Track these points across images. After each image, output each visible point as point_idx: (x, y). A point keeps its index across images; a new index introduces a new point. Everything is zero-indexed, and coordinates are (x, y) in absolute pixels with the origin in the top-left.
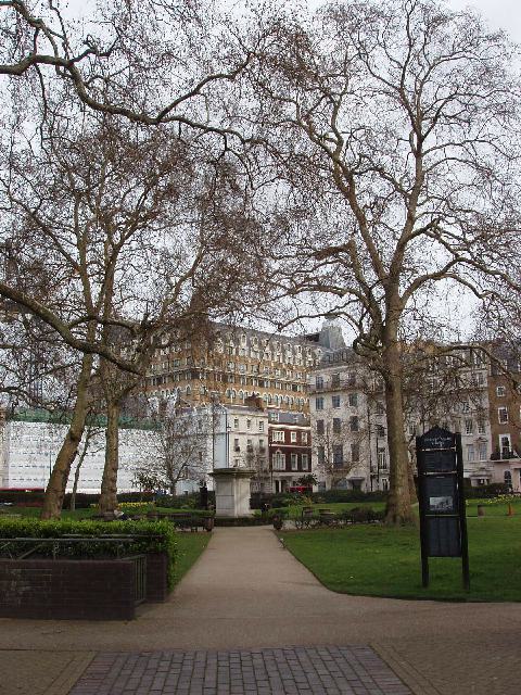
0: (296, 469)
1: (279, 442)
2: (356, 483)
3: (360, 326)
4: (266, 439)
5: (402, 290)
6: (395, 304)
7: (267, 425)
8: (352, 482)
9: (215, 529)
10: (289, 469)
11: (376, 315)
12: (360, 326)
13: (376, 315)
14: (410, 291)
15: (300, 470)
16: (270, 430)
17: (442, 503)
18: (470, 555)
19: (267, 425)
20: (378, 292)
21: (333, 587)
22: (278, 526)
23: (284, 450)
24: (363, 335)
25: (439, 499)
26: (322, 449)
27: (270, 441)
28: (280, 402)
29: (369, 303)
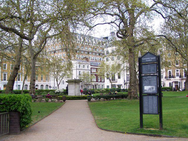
0: (100, 81)
1: (94, 73)
2: (119, 86)
3: (119, 26)
4: (90, 72)
5: (135, 15)
6: (133, 21)
7: (90, 67)
8: (118, 86)
9: (66, 101)
10: (97, 81)
11: (125, 24)
12: (119, 26)
13: (125, 24)
14: (138, 16)
15: (101, 82)
16: (91, 68)
17: (150, 89)
18: (163, 114)
19: (90, 67)
20: (127, 15)
21: (138, 132)
22: (89, 100)
23: (96, 75)
24: (120, 30)
25: (149, 87)
26: (108, 75)
27: (91, 72)
28: (94, 59)
29: (122, 19)
